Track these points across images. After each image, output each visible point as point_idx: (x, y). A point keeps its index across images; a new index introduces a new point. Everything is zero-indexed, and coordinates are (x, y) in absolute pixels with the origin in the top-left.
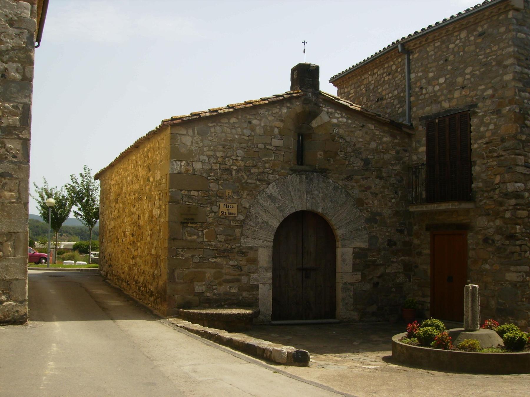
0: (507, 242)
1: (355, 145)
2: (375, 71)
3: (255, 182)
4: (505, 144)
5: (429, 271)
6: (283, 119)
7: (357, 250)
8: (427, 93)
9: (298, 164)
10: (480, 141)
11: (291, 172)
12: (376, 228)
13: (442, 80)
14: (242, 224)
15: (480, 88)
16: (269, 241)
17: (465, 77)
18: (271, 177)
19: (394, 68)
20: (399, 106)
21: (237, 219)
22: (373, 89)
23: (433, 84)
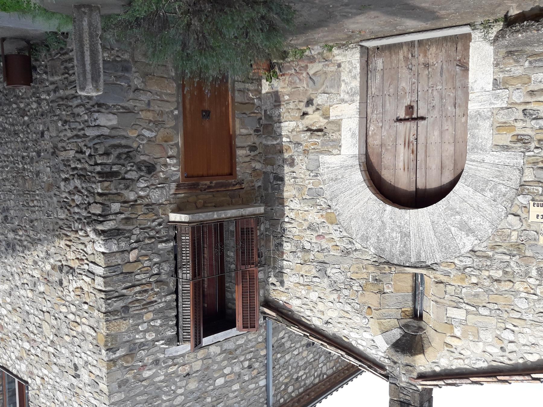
0: (115, 168)
1: (339, 297)
2: (317, 380)
3: (496, 256)
4: (122, 305)
5: (238, 126)
6: (446, 348)
7: (335, 151)
8: (242, 362)
9: (422, 275)
10: (161, 305)
11: (434, 267)
12: (309, 183)
13: (220, 381)
14: (522, 188)
15: (162, 378)
16: (474, 161)
17: (185, 389)
18: (468, 262)
19: (290, 389)
20: (283, 340)
21: (529, 197)
22: (320, 357)
23: (232, 375)
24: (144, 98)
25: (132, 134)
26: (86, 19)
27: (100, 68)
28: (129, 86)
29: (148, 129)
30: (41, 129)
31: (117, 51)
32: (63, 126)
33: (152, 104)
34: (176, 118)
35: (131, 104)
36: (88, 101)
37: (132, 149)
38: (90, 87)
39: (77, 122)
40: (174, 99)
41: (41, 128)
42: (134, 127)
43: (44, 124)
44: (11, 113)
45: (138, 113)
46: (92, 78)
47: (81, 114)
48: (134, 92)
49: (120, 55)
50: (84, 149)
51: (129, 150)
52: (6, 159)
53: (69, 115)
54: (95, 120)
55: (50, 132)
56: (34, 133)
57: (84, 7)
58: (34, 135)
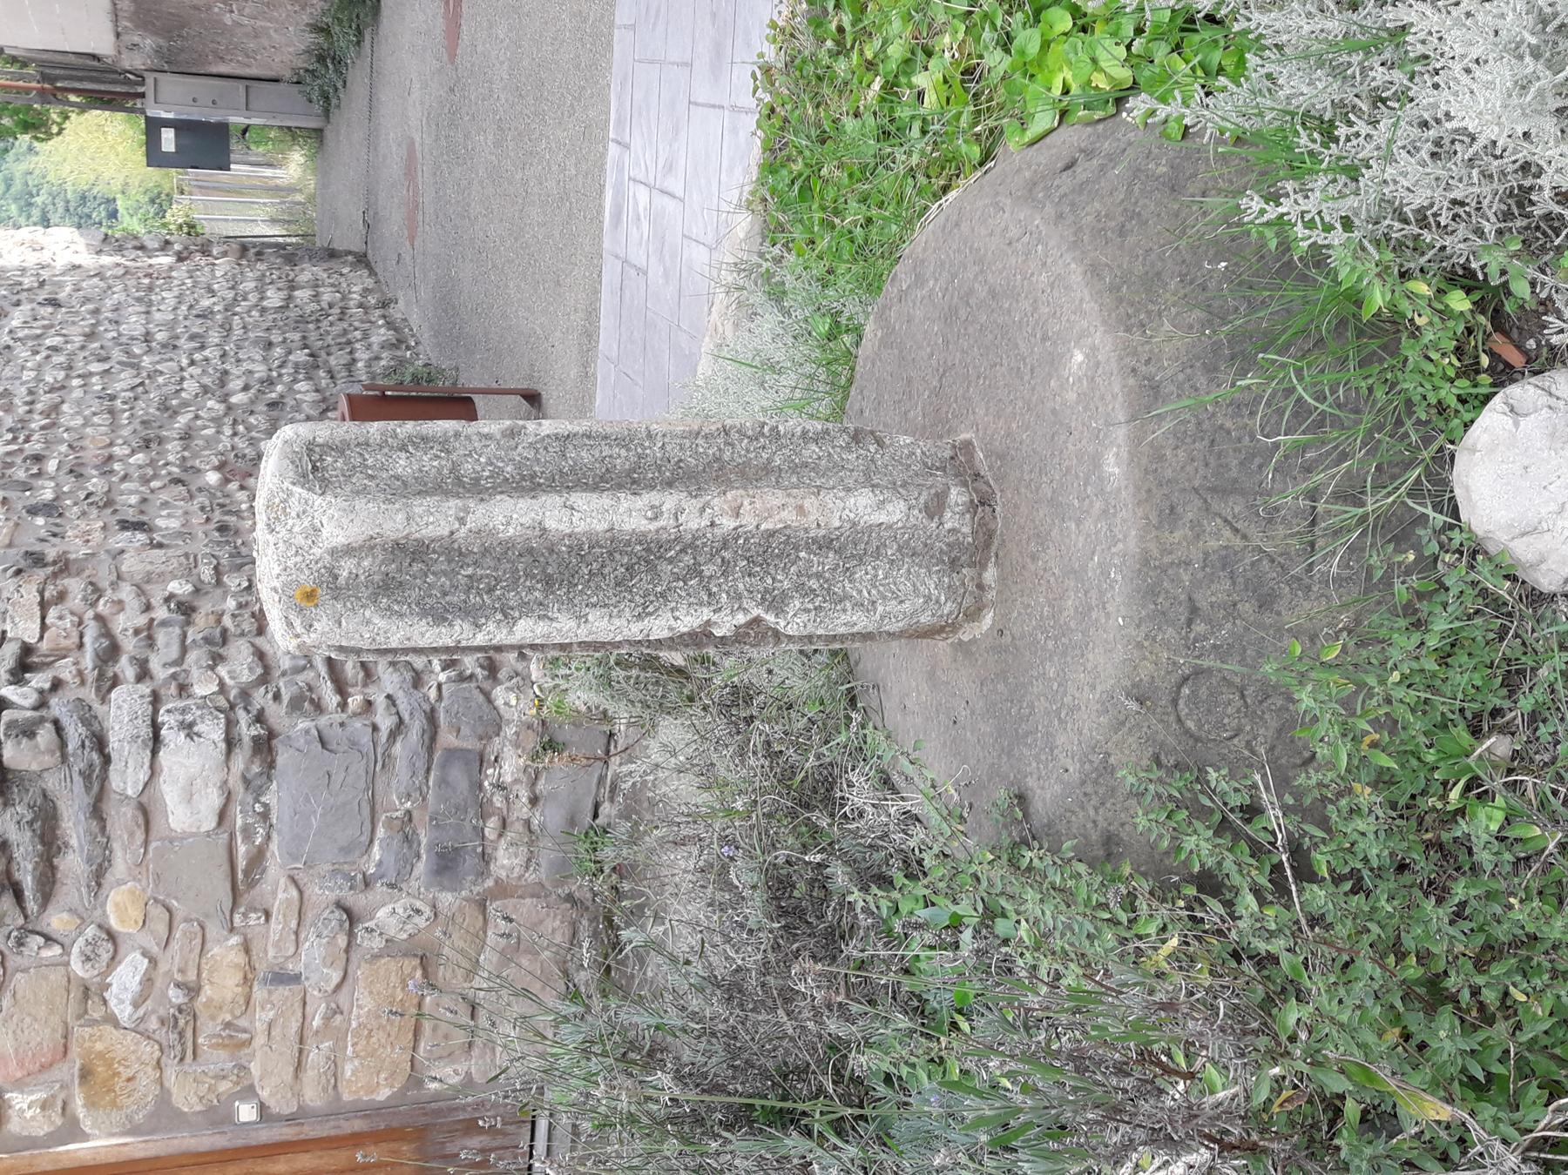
24: (315, 957)
25: (120, 906)
26: (895, 512)
27: (508, 615)
28: (367, 883)
29: (148, 981)
30: (160, 522)
31: (528, 823)
32: (167, 600)
33: (283, 991)
34: (219, 1116)
35: (276, 888)
36: (286, 697)
37: (32, 906)
38: (337, 522)
39: (184, 650)
40: (313, 1096)
41: (166, 523)
42: (157, 912)
43: (185, 534)
44: (235, 434)
45: (232, 929)
46: (412, 552)
47: (222, 670)
48: (340, 905)
49: (510, 835)
50: (40, 680)
51: (28, 894)
52: (39, 406)
53: (219, 621)
54: (188, 728)
55: (139, 551)
56: (144, 500)
57: (972, 507)
58: (133, 499)
